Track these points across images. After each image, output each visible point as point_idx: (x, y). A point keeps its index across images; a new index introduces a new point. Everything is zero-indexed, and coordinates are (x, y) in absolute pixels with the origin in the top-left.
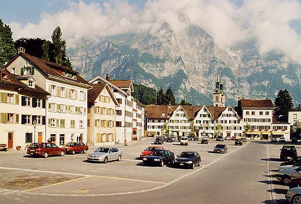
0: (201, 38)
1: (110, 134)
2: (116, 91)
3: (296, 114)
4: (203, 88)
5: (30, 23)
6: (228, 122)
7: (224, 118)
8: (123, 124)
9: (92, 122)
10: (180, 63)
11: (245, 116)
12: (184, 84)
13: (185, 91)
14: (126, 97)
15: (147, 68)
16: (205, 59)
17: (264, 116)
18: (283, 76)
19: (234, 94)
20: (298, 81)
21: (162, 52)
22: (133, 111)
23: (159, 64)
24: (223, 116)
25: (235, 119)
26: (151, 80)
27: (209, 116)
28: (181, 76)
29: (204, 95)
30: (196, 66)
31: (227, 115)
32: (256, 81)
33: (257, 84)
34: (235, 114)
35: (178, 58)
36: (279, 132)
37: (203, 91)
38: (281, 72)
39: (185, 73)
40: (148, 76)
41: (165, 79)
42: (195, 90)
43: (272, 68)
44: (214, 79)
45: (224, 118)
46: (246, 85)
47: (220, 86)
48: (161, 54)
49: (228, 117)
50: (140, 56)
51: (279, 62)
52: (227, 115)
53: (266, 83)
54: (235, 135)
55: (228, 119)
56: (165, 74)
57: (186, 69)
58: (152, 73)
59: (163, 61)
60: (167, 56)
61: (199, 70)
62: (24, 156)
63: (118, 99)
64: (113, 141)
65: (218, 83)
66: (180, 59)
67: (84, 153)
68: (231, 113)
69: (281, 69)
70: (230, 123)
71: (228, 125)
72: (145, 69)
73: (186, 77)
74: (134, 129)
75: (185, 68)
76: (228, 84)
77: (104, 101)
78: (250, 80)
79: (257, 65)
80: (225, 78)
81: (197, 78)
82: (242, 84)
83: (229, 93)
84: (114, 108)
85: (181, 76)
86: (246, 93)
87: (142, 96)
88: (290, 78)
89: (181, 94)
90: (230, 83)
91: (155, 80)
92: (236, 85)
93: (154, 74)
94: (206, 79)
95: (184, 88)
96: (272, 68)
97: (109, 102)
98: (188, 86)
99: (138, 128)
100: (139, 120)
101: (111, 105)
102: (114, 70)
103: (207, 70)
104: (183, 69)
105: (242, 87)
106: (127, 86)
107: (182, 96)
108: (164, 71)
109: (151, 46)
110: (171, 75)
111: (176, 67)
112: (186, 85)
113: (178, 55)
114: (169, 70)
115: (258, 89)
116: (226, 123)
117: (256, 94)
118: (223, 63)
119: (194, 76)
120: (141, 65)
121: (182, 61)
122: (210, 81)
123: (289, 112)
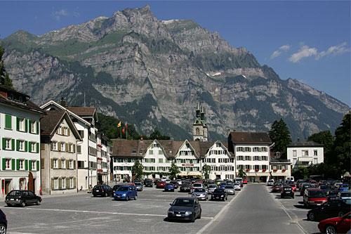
0: (173, 55)
1: (71, 178)
2: (75, 120)
3: (296, 151)
4: (177, 117)
5: (307, 47)
6: (217, 161)
7: (213, 156)
8: (86, 165)
9: (47, 163)
10: (147, 85)
11: (238, 154)
12: (153, 112)
13: (154, 121)
14: (89, 129)
15: (104, 91)
16: (179, 81)
17: (260, 154)
19: (215, 126)
20: (290, 110)
21: (123, 71)
22: (87, 147)
23: (120, 87)
24: (210, 154)
25: (226, 157)
27: (193, 154)
28: (148, 102)
29: (178, 126)
30: (168, 90)
31: (216, 152)
32: (242, 110)
33: (243, 114)
34: (226, 151)
35: (144, 79)
36: (279, 173)
37: (177, 121)
38: (271, 99)
40: (106, 102)
41: (129, 106)
42: (167, 120)
43: (260, 94)
44: (191, 106)
45: (213, 156)
46: (230, 114)
47: (200, 115)
48: (123, 73)
49: (217, 154)
50: (95, 75)
51: (268, 87)
52: (216, 152)
53: (254, 113)
54: (226, 177)
55: (217, 157)
56: (128, 99)
57: (156, 92)
58: (111, 98)
59: (126, 82)
60: (130, 76)
61: (170, 95)
62: (295, 206)
63: (79, 131)
64: (75, 187)
65: (198, 112)
66: (147, 80)
67: (37, 204)
68: (220, 149)
69: (270, 96)
70: (219, 162)
71: (218, 164)
72: (101, 92)
73: (156, 104)
74: (99, 170)
75: (153, 92)
76: (209, 113)
77: (62, 136)
78: (235, 108)
79: (243, 91)
80: (204, 105)
81: (170, 104)
82: (225, 113)
84: (74, 143)
85: (148, 102)
86: (231, 123)
87: (107, 131)
88: (281, 107)
89: (149, 125)
90: (211, 112)
91: (115, 107)
92: (218, 115)
93: (114, 100)
94: (180, 107)
95: (153, 117)
96: (260, 94)
97: (69, 135)
98: (157, 114)
99: (105, 170)
100: (105, 160)
101: (71, 139)
102: (61, 92)
103: (183, 95)
104: (152, 93)
105: (225, 116)
106: (89, 114)
107: (151, 128)
108: (127, 96)
109: (110, 64)
110: (135, 101)
111: (142, 90)
112: (156, 114)
113: (145, 74)
114: (133, 93)
115: (244, 119)
116: (215, 162)
117: (243, 126)
118: (201, 86)
119: (165, 102)
120: (97, 87)
121: (150, 84)
122: (185, 109)
123: (288, 149)
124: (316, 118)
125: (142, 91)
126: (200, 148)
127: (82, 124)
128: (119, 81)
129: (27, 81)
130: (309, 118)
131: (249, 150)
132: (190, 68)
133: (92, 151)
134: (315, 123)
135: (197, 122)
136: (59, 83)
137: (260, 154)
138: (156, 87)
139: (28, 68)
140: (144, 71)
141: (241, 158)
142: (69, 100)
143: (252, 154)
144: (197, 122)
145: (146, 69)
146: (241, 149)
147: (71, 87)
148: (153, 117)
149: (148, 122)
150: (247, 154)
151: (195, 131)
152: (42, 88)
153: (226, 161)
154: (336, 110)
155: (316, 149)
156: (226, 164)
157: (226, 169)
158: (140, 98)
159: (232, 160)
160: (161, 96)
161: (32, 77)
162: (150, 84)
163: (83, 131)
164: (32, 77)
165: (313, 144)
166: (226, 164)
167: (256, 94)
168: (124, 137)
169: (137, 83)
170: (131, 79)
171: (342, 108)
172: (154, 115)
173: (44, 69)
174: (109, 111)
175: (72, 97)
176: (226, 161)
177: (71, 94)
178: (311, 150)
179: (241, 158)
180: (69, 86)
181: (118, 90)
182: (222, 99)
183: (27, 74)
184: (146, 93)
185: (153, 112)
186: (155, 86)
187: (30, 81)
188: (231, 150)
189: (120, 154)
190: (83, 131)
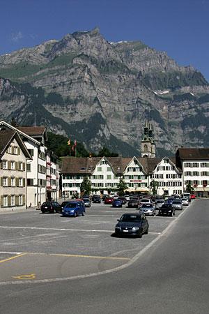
11: (186, 169)
12: (102, 130)
19: (163, 142)
23: (70, 107)
26: (60, 126)
30: (116, 108)
39: (103, 116)
41: (79, 125)
48: (73, 94)
56: (78, 118)
59: (76, 102)
66: (96, 99)
73: (104, 122)
75: (102, 111)
79: (190, 108)
83: (158, 141)
90: (159, 129)
94: (129, 125)
95: (101, 135)
102: (12, 113)
104: (101, 112)
108: (76, 115)
110: (85, 119)
113: (94, 94)
119: (114, 121)
125: (93, 109)
128: (68, 101)
131: (196, 165)
132: (138, 87)
133: (41, 169)
135: (145, 139)
136: (10, 104)
140: (94, 91)
141: (189, 173)
142: (20, 120)
144: (145, 139)
145: (95, 89)
146: (189, 165)
147: (23, 107)
148: (101, 135)
149: (97, 140)
151: (143, 148)
153: (173, 176)
156: (174, 180)
157: (174, 184)
159: (180, 176)
160: (110, 114)
162: (99, 103)
166: (174, 180)
167: (203, 110)
168: (73, 155)
169: (86, 103)
170: (81, 99)
172: (103, 134)
174: (59, 130)
175: (22, 118)
176: (173, 176)
179: (189, 173)
180: (20, 107)
182: (170, 117)
184: (95, 112)
185: (102, 130)
186: (104, 105)
188: (179, 166)
189: (69, 172)
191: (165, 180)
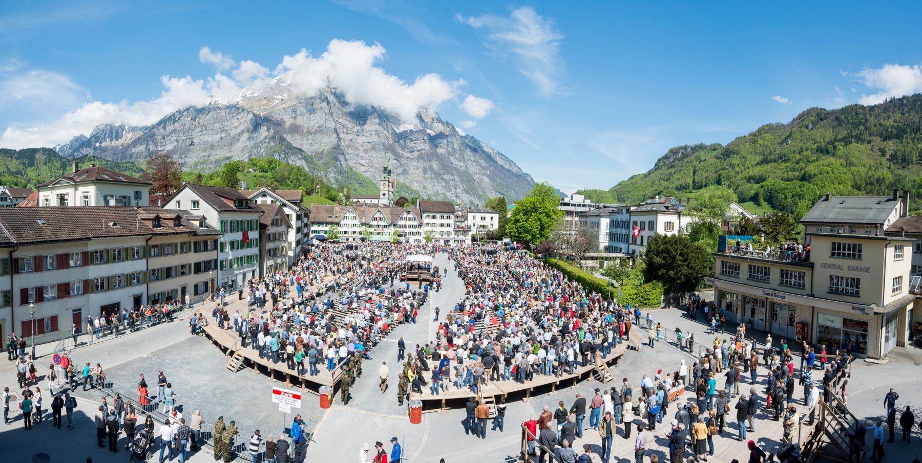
11: (425, 221)
15: (295, 141)
18: (452, 158)
23: (310, 137)
26: (300, 156)
60: (319, 127)
63: (288, 215)
66: (336, 130)
124: (488, 172)
126: (391, 215)
127: (291, 208)
129: (225, 135)
130: (482, 172)
131: (434, 217)
134: (487, 176)
135: (385, 178)
137: (445, 221)
138: (342, 137)
139: (225, 123)
141: (428, 224)
143: (438, 221)
144: (385, 178)
148: (339, 166)
150: (434, 221)
152: (239, 140)
153: (415, 227)
154: (506, 167)
155: (492, 215)
158: (328, 147)
159: (420, 226)
161: (230, 131)
163: (291, 215)
164: (230, 131)
165: (490, 211)
171: (511, 165)
172: (341, 164)
173: (241, 123)
174: (299, 159)
176: (415, 227)
177: (265, 145)
178: (488, 216)
181: (308, 140)
183: (225, 128)
186: (342, 136)
187: (229, 135)
190: (291, 215)
191: (407, 230)
